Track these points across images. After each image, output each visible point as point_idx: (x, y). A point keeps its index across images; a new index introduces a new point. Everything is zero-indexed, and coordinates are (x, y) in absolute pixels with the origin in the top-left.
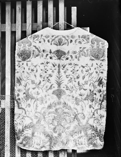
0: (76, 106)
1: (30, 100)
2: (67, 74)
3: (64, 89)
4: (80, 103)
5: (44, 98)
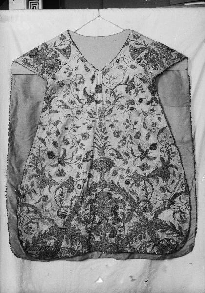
0: (134, 188)
1: (47, 188)
2: (115, 129)
3: (112, 158)
4: (142, 183)
5: (75, 179)
